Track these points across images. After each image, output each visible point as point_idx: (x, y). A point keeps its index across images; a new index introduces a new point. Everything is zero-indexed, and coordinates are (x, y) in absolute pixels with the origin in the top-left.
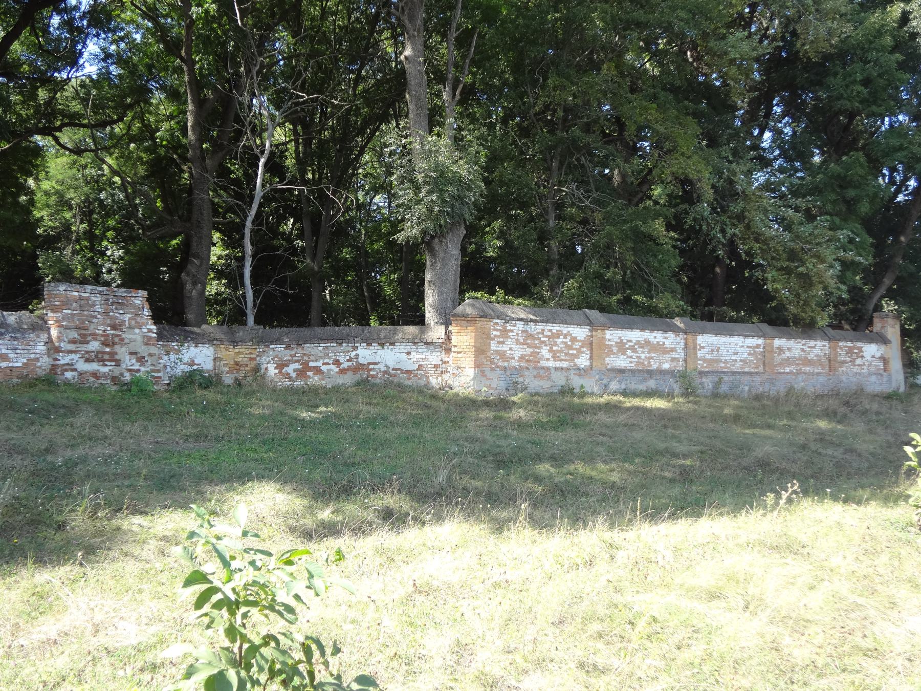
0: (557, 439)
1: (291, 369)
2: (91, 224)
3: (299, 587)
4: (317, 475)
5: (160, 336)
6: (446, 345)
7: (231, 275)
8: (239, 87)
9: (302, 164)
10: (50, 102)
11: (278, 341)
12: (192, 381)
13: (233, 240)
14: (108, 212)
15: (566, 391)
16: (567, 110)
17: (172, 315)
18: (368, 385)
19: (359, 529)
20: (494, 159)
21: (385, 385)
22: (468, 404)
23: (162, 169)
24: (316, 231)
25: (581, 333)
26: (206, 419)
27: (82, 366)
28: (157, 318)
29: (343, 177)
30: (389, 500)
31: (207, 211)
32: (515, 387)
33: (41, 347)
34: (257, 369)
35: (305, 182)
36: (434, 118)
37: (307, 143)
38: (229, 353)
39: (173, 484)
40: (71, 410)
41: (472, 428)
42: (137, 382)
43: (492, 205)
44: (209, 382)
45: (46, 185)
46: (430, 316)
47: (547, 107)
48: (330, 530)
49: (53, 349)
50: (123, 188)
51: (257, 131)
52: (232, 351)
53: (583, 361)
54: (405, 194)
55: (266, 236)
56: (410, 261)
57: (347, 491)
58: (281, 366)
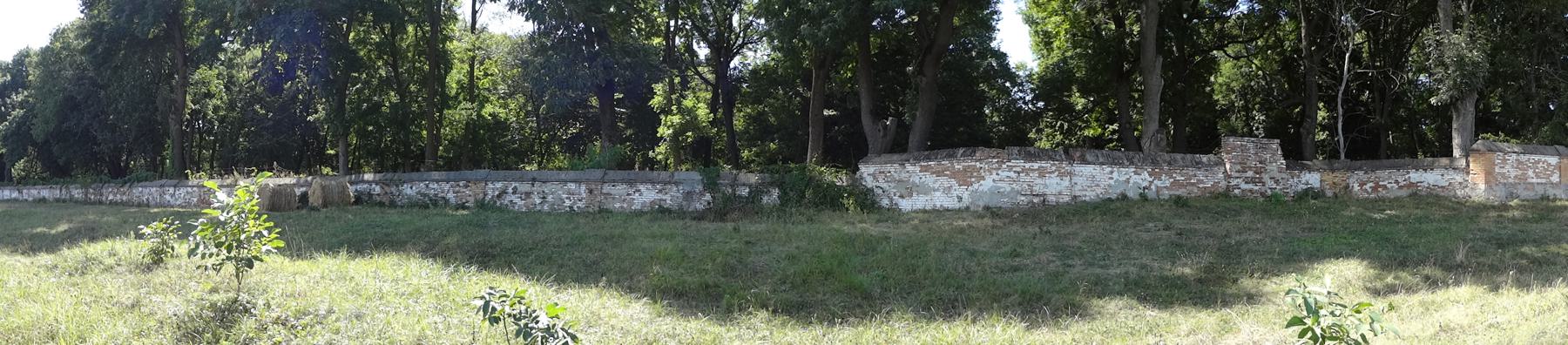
0: (1537, 229)
1: (1367, 187)
2: (1247, 102)
3: (1365, 329)
4: (1384, 254)
5: (1288, 167)
6: (1467, 171)
7: (1330, 127)
8: (1332, 9)
9: (1372, 55)
10: (1221, 30)
11: (1360, 169)
12: (1308, 194)
13: (1331, 107)
14: (1256, 94)
15: (1545, 198)
16: (1542, 18)
17: (1295, 155)
18: (1417, 196)
19: (1410, 290)
20: (1496, 49)
21: (1429, 195)
22: (1483, 208)
23: (1288, 65)
24: (1383, 99)
25: (1553, 160)
26: (1315, 218)
27: (1244, 186)
28: (1286, 157)
29: (1399, 65)
30: (1428, 271)
31: (1315, 89)
32: (1511, 196)
33: (1221, 175)
34: (1347, 187)
35: (1375, 67)
36: (1456, 24)
37: (1376, 43)
38: (1330, 177)
39: (1295, 257)
40: (1238, 213)
41: (1483, 223)
42: (1275, 195)
43: (1494, 79)
44: (1317, 194)
45: (1220, 80)
46: (1457, 153)
47: (1529, 14)
48: (1392, 290)
49: (1228, 177)
50: (1264, 78)
51: (1345, 37)
52: (1331, 176)
53: (1555, 178)
54: (1439, 72)
55: (1351, 101)
56: (1443, 116)
57: (1403, 265)
58: (1361, 185)
